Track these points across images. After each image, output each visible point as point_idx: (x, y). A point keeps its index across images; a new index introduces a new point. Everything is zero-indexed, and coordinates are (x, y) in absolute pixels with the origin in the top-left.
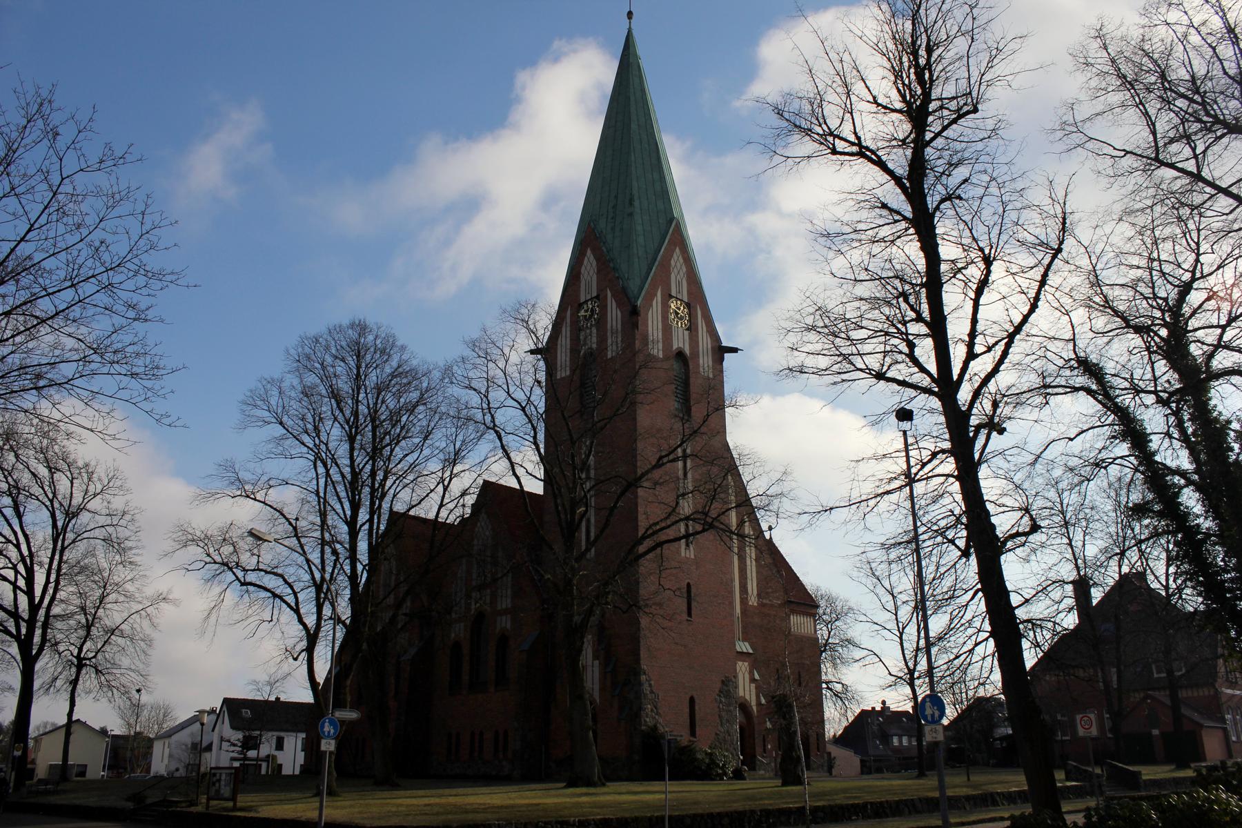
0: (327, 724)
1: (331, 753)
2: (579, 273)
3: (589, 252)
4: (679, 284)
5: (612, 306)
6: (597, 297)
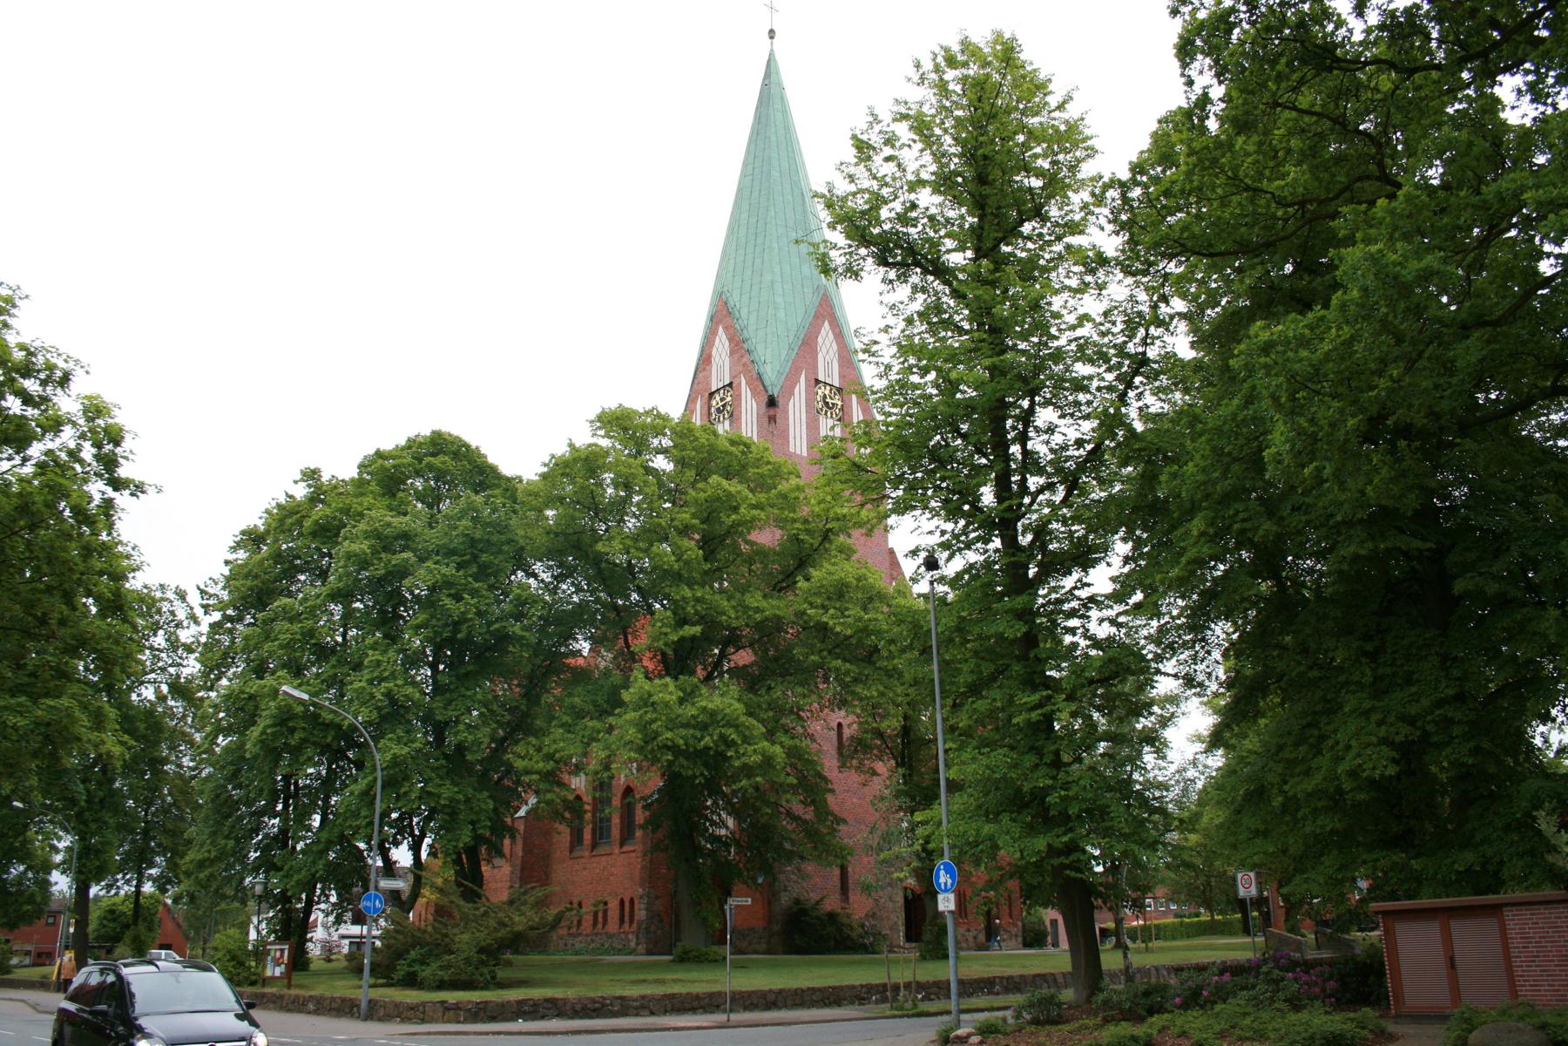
0: (942, 872)
1: (951, 912)
2: (710, 356)
3: (721, 330)
4: (828, 364)
5: (746, 392)
6: (730, 385)
